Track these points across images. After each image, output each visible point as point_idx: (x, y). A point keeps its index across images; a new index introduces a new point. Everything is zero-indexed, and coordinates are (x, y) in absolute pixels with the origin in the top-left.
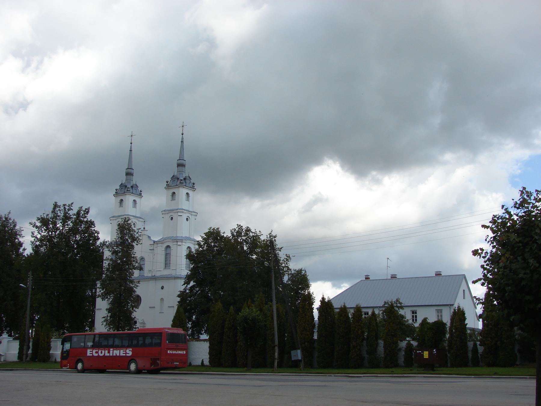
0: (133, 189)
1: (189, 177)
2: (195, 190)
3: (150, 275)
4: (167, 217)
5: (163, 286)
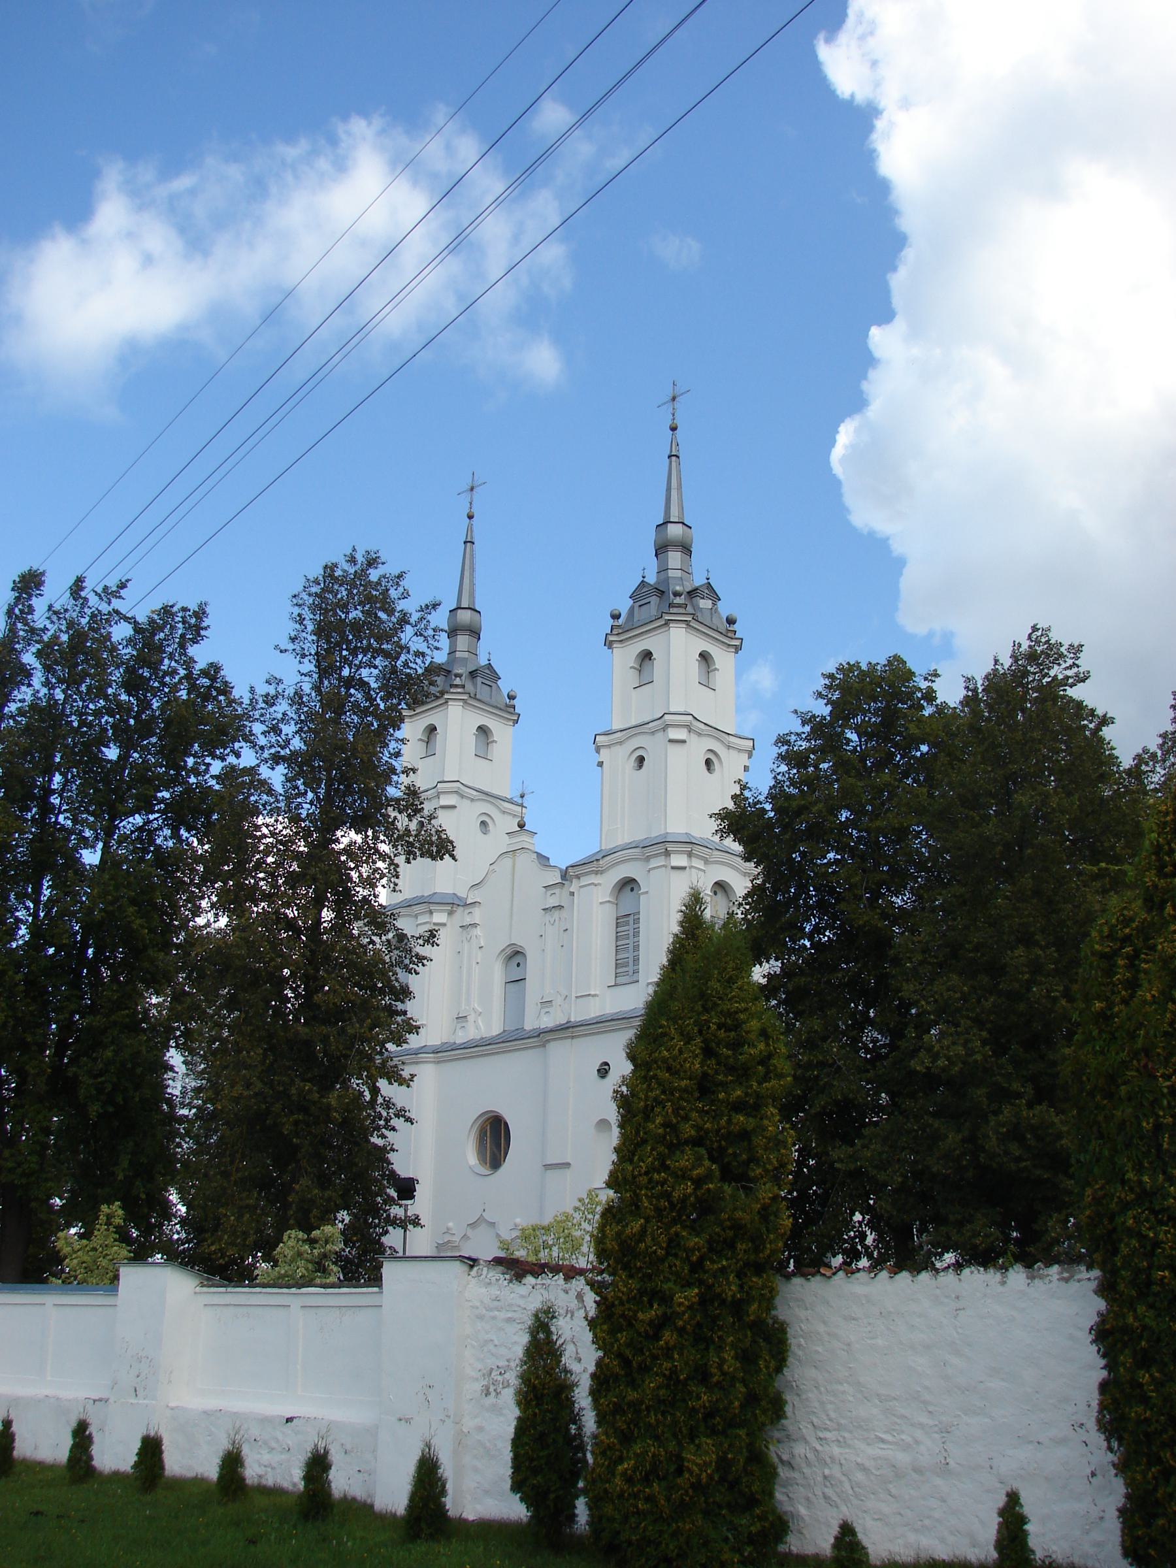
0: (479, 683)
1: (709, 586)
2: (737, 643)
3: (547, 1022)
4: (619, 759)
5: (607, 1064)
